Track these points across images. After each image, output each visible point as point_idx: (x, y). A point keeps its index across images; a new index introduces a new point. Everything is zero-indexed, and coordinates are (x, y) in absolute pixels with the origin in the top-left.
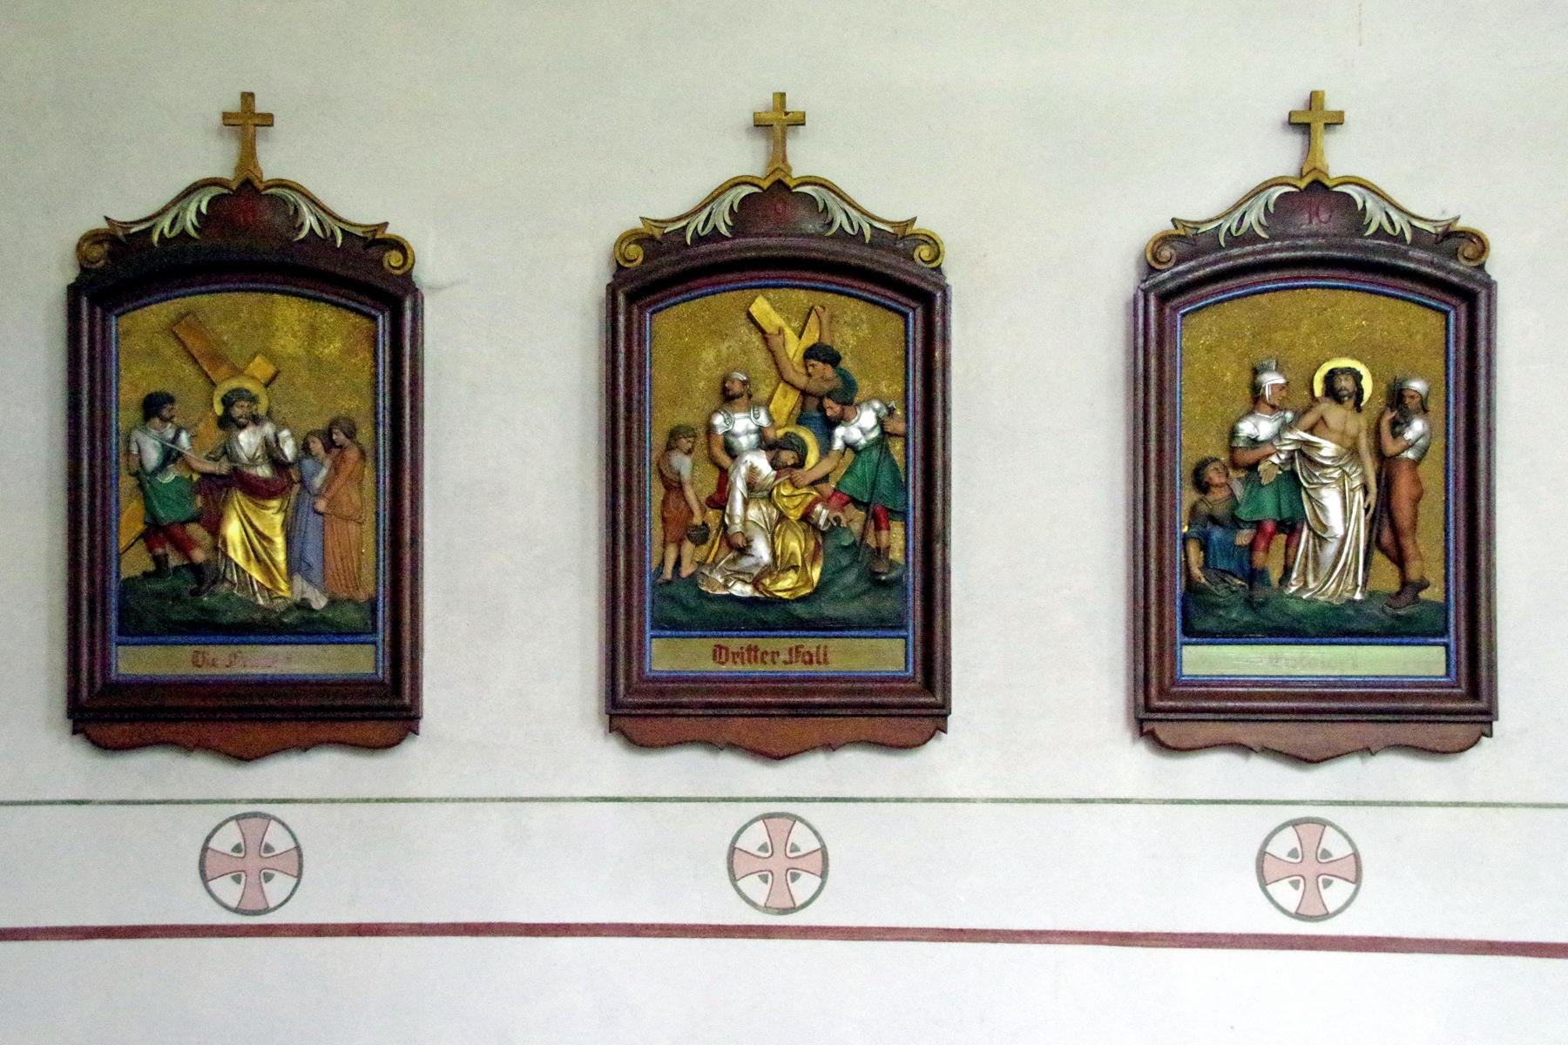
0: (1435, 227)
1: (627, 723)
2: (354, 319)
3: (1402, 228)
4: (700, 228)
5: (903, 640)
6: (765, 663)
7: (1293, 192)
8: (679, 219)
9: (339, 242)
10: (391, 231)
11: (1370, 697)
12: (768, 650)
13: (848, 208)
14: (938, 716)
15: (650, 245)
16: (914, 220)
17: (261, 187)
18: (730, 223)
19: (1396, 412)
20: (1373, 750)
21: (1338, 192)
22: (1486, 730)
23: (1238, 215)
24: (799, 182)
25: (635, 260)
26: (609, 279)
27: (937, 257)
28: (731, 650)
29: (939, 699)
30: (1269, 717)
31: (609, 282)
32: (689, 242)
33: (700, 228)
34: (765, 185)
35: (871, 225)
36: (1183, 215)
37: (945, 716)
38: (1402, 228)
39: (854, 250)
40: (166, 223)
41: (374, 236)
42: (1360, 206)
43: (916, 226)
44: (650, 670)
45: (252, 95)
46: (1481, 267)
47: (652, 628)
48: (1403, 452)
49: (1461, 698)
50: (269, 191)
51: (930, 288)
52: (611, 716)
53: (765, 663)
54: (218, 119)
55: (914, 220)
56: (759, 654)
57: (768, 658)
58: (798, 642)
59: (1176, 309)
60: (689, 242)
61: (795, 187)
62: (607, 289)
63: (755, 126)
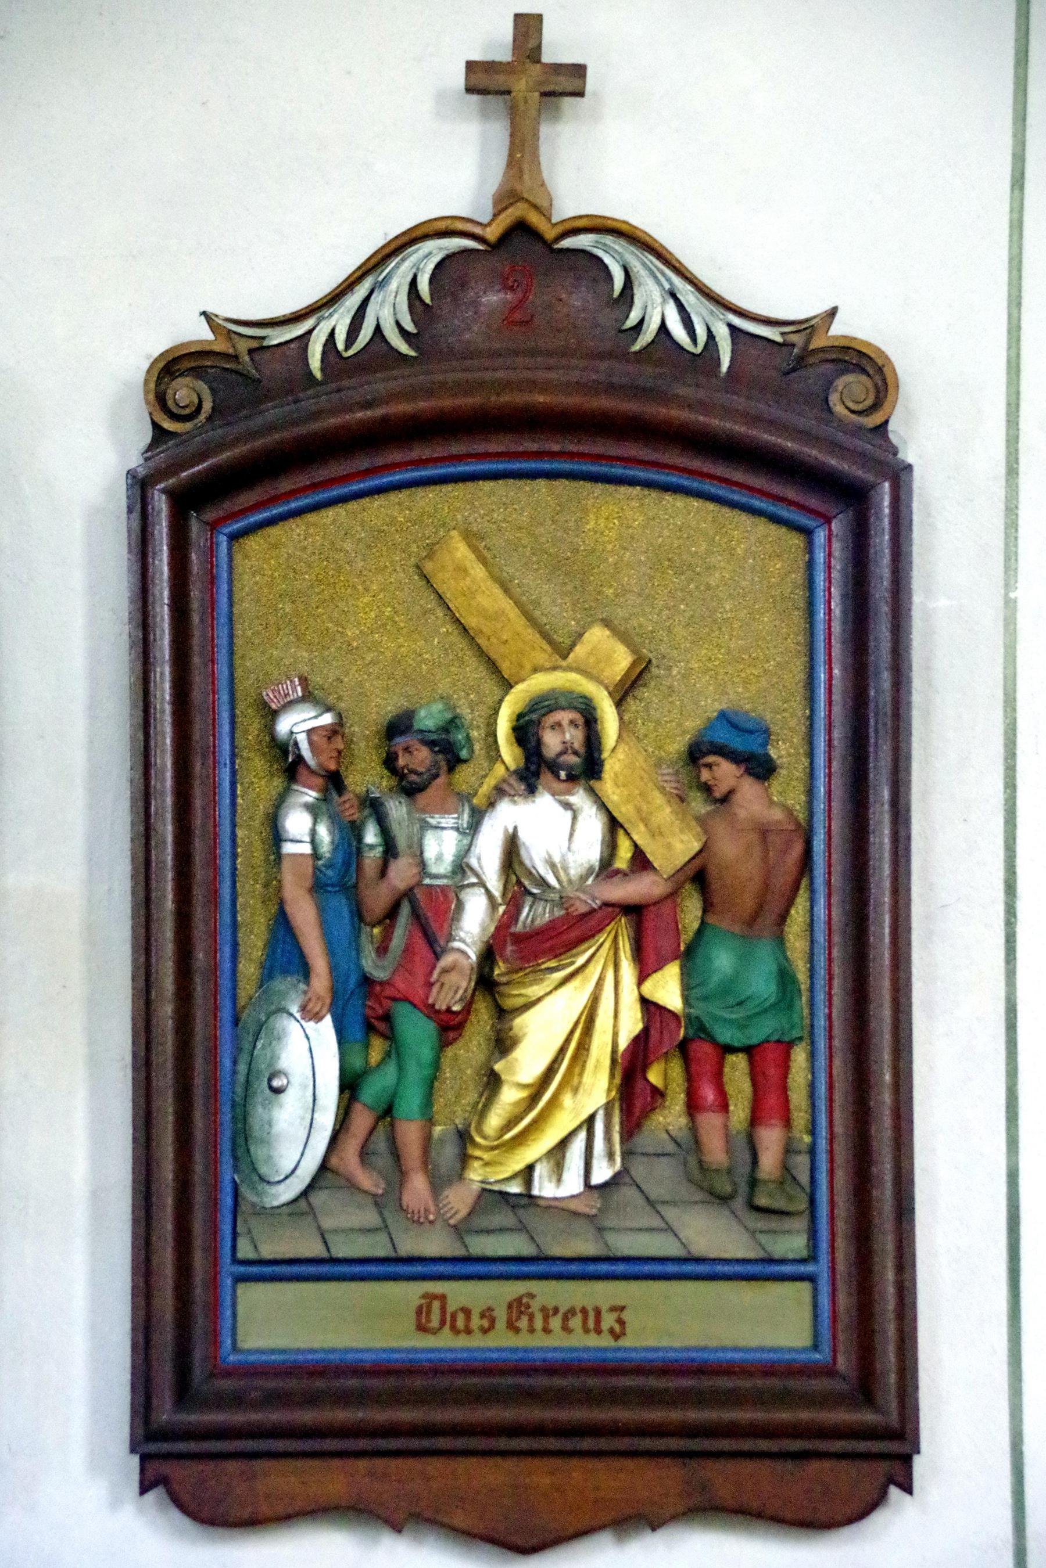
0: (783, 334)
1: (183, 1472)
3: (711, 336)
5: (805, 1287)
6: (517, 1330)
7: (478, 250)
8: (296, 318)
16: (833, 313)
17: (550, 234)
18: (410, 327)
19: (392, 803)
21: (568, 250)
23: (353, 301)
25: (200, 407)
26: (134, 460)
27: (875, 407)
31: (133, 465)
32: (318, 375)
34: (492, 234)
36: (226, 309)
38: (711, 336)
39: (379, 384)
40: (340, 320)
41: (808, 341)
43: (838, 329)
44: (235, 1348)
45: (537, 19)
48: (410, 902)
50: (568, 243)
51: (859, 473)
52: (144, 1459)
53: (517, 1330)
54: (458, 78)
55: (833, 313)
57: (555, 1323)
60: (318, 375)
63: (470, 90)
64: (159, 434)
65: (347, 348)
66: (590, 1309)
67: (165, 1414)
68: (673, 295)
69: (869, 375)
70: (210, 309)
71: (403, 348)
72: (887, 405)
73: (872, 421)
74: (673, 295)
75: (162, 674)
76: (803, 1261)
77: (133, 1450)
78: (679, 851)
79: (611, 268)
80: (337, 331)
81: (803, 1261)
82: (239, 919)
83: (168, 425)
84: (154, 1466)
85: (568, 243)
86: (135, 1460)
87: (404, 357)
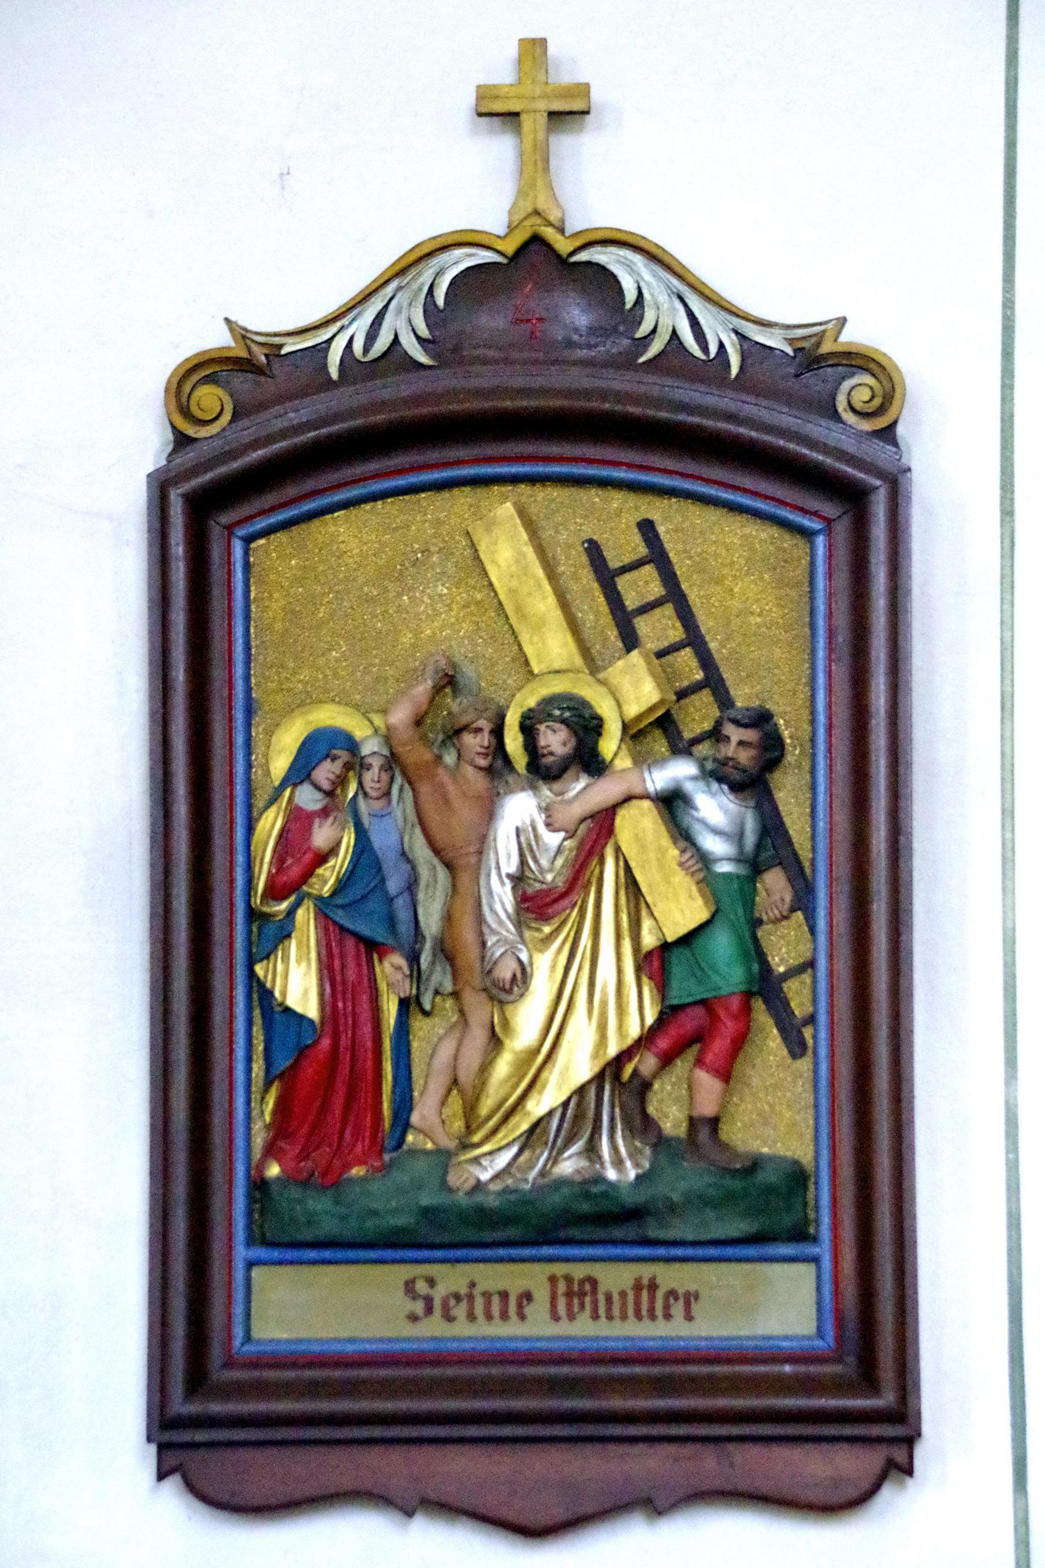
2: (762, 534)
3: (721, 345)
4: (358, 347)
9: (734, 370)
10: (851, 336)
11: (313, 1389)
12: (681, 1291)
13: (696, 304)
14: (892, 1441)
15: (243, 382)
16: (842, 321)
17: (563, 246)
18: (424, 332)
20: (660, 1503)
22: (899, 1454)
24: (578, 243)
28: (602, 1289)
29: (886, 1400)
30: (632, 1430)
32: (334, 372)
33: (358, 347)
34: (510, 247)
35: (742, 337)
37: (910, 1440)
38: (721, 345)
40: (359, 327)
42: (630, 296)
43: (849, 336)
45: (543, 42)
46: (888, 434)
47: (250, 1242)
49: (837, 1386)
52: (163, 1448)
56: (660, 1295)
58: (646, 1271)
59: (230, 528)
60: (334, 372)
61: (573, 253)
62: (148, 483)
64: (182, 441)
65: (366, 350)
66: (603, 1319)
67: (179, 1407)
68: (681, 299)
69: (874, 375)
70: (233, 318)
71: (422, 358)
72: (896, 402)
73: (881, 423)
74: (681, 299)
75: (178, 568)
76: (819, 1269)
77: (149, 1440)
78: (684, 636)
79: (620, 279)
80: (355, 338)
81: (819, 1269)
82: (254, 695)
83: (191, 431)
84: (172, 1460)
85: (583, 256)
86: (153, 1449)
87: (421, 366)
